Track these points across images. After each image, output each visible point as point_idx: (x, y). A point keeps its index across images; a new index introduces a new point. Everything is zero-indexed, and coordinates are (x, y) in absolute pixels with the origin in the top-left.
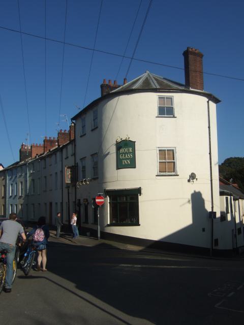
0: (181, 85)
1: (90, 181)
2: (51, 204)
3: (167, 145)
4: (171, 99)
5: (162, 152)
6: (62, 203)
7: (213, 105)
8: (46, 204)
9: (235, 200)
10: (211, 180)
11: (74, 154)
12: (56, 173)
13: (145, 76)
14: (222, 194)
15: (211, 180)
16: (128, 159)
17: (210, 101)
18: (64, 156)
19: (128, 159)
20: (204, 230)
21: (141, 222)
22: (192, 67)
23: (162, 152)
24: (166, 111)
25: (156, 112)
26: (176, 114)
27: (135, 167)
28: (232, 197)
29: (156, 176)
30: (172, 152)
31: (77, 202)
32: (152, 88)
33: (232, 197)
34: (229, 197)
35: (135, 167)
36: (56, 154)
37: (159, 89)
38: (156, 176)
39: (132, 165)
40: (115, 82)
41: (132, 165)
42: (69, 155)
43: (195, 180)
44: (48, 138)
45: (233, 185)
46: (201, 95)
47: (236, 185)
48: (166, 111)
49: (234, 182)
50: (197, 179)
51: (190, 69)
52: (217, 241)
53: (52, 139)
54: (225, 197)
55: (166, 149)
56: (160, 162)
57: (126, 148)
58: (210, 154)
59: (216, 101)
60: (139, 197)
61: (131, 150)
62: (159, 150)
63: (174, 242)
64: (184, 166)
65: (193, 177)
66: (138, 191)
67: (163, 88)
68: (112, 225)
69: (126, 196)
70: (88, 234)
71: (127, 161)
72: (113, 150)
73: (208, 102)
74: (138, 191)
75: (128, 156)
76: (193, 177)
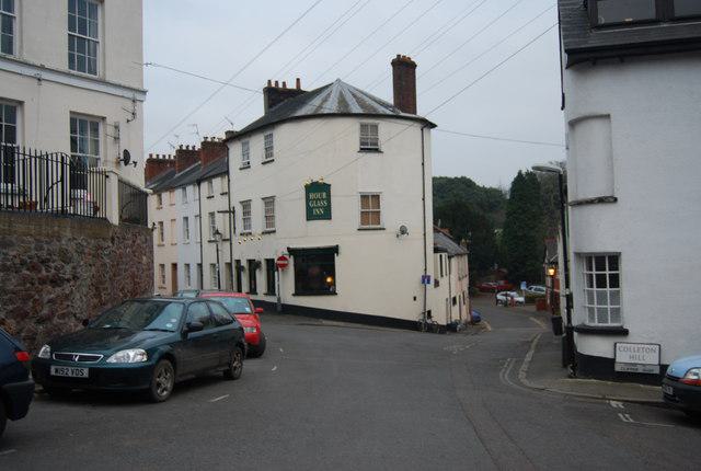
0: (385, 105)
1: (530, 300)
2: (175, 266)
4: (376, 127)
5: (364, 197)
6: (200, 265)
8: (188, 265)
11: (227, 194)
12: (186, 219)
14: (436, 250)
20: (415, 299)
23: (364, 197)
24: (370, 147)
30: (376, 197)
31: (234, 265)
35: (330, 219)
39: (327, 215)
40: (284, 83)
41: (327, 215)
42: (217, 194)
48: (370, 147)
51: (561, 348)
52: (429, 312)
53: (161, 157)
60: (336, 258)
64: (390, 216)
65: (403, 231)
70: (279, 308)
74: (335, 250)
76: (403, 231)
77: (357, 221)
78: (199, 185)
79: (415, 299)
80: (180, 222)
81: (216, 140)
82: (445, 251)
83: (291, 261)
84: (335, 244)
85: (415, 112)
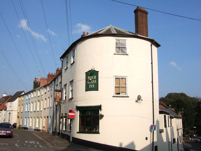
3: (120, 74)
6: (171, 141)
7: (155, 48)
9: (171, 118)
10: (153, 102)
11: (61, 83)
13: (108, 28)
14: (161, 112)
15: (153, 102)
16: (93, 84)
17: (153, 46)
18: (56, 84)
19: (93, 84)
20: (147, 139)
21: (101, 130)
22: (140, 20)
24: (121, 49)
25: (114, 50)
26: (128, 51)
27: (98, 90)
28: (167, 116)
29: (113, 97)
30: (124, 79)
32: (113, 33)
33: (169, 116)
34: (167, 116)
35: (98, 90)
36: (52, 83)
37: (116, 34)
38: (113, 97)
39: (96, 89)
41: (96, 89)
42: (59, 84)
43: (141, 101)
44: (51, 74)
45: (172, 109)
46: (147, 40)
47: (173, 109)
48: (121, 49)
49: (172, 107)
50: (142, 100)
54: (163, 115)
55: (120, 77)
56: (116, 87)
57: (92, 75)
58: (152, 82)
59: (157, 45)
60: (100, 121)
61: (95, 78)
62: (115, 78)
63: (89, 39)
64: (132, 90)
66: (99, 107)
67: (120, 34)
68: (80, 132)
69: (91, 111)
71: (92, 86)
72: (84, 77)
73: (151, 45)
74: (99, 107)
75: (92, 86)
76: (139, 98)
77: (113, 92)
78: (46, 87)
79: (147, 139)
80: (46, 117)
81: (53, 74)
82: (168, 114)
83: (78, 113)
84: (99, 104)
85: (147, 36)
